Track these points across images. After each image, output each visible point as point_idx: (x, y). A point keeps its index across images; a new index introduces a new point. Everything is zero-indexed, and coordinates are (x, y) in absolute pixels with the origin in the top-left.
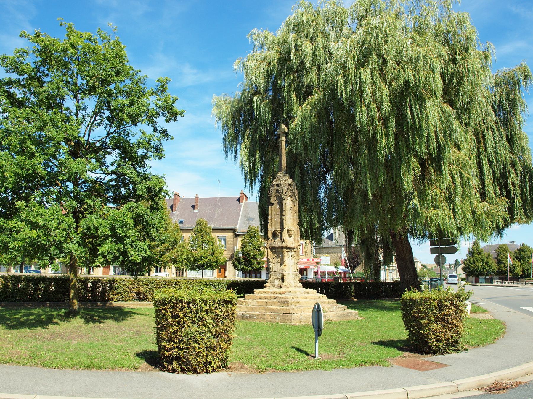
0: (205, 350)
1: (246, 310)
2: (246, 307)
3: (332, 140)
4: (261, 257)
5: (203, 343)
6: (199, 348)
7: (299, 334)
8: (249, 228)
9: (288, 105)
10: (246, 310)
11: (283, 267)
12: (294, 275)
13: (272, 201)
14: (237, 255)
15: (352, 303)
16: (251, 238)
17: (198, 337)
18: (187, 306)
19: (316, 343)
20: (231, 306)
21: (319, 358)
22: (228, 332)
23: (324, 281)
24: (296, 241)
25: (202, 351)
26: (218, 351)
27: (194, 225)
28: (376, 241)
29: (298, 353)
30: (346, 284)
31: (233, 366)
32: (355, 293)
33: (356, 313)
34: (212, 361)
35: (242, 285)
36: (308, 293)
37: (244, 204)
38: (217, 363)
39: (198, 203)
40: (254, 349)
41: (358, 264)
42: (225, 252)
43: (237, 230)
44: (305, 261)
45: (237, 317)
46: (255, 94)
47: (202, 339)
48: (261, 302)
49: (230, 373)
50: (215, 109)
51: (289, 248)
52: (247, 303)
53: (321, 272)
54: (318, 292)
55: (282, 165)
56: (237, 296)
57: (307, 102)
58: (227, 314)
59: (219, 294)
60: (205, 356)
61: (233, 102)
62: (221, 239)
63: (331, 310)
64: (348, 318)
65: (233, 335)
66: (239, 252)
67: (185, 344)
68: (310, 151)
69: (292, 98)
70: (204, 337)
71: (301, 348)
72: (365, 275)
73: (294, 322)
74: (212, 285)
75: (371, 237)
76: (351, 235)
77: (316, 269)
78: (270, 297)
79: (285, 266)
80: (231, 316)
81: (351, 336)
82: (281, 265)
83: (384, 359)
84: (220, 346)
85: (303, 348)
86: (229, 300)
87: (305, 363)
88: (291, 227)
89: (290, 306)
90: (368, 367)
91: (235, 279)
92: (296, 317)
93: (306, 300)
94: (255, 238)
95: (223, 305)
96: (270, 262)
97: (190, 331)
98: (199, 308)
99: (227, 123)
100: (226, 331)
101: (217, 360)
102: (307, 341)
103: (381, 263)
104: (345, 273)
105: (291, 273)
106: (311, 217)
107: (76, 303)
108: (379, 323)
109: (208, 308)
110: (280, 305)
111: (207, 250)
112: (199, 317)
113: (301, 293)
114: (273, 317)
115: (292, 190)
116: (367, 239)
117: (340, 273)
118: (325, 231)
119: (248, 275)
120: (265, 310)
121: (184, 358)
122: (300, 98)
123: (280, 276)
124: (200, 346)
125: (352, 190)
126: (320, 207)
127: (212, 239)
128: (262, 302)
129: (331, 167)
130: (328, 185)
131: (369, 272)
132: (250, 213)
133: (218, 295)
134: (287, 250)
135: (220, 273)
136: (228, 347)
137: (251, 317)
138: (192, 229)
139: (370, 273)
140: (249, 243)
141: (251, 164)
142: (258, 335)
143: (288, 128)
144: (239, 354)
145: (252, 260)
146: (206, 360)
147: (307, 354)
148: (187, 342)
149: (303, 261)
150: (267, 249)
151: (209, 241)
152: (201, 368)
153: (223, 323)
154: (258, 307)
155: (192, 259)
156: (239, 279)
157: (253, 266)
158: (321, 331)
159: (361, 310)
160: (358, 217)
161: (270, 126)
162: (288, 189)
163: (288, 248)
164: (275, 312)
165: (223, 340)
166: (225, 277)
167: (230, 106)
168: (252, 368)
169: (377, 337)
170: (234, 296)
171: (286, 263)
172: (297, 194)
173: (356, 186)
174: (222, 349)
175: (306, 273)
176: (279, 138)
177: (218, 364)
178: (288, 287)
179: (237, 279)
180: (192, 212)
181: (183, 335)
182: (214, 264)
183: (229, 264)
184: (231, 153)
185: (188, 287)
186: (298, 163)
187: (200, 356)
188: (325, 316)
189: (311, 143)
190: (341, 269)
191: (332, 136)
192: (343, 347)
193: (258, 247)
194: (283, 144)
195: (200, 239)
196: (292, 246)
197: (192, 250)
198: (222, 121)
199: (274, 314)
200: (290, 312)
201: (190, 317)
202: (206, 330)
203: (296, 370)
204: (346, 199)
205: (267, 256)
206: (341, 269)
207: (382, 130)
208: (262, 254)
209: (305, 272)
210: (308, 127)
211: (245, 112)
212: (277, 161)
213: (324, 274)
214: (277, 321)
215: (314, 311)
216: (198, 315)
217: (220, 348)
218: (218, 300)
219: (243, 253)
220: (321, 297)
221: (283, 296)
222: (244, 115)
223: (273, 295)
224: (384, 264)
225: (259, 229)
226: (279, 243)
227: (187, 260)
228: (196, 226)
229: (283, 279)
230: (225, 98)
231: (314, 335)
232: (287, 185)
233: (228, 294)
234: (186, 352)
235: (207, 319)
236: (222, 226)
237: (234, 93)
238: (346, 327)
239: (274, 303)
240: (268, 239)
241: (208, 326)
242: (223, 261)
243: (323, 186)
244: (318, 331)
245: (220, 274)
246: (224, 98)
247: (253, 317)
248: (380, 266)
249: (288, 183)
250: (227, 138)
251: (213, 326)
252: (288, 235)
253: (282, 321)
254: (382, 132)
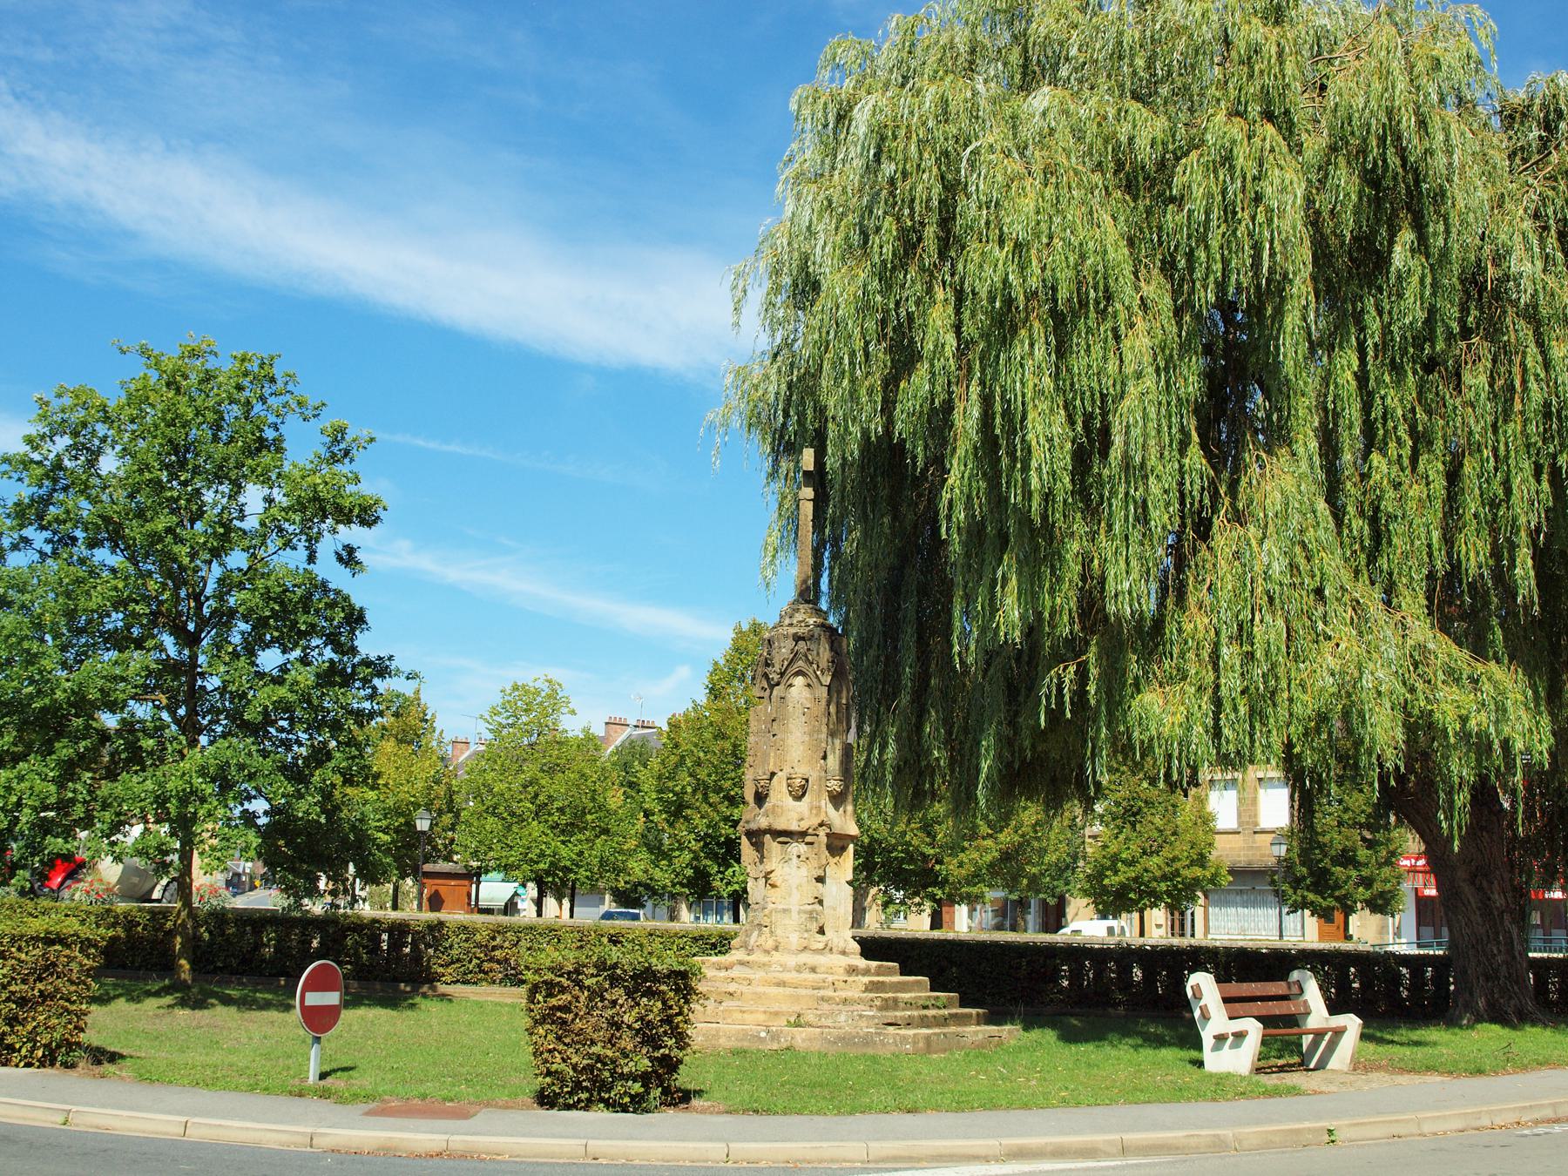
12: (805, 916)
105: (795, 909)
107: (187, 967)
166: (1348, 938)
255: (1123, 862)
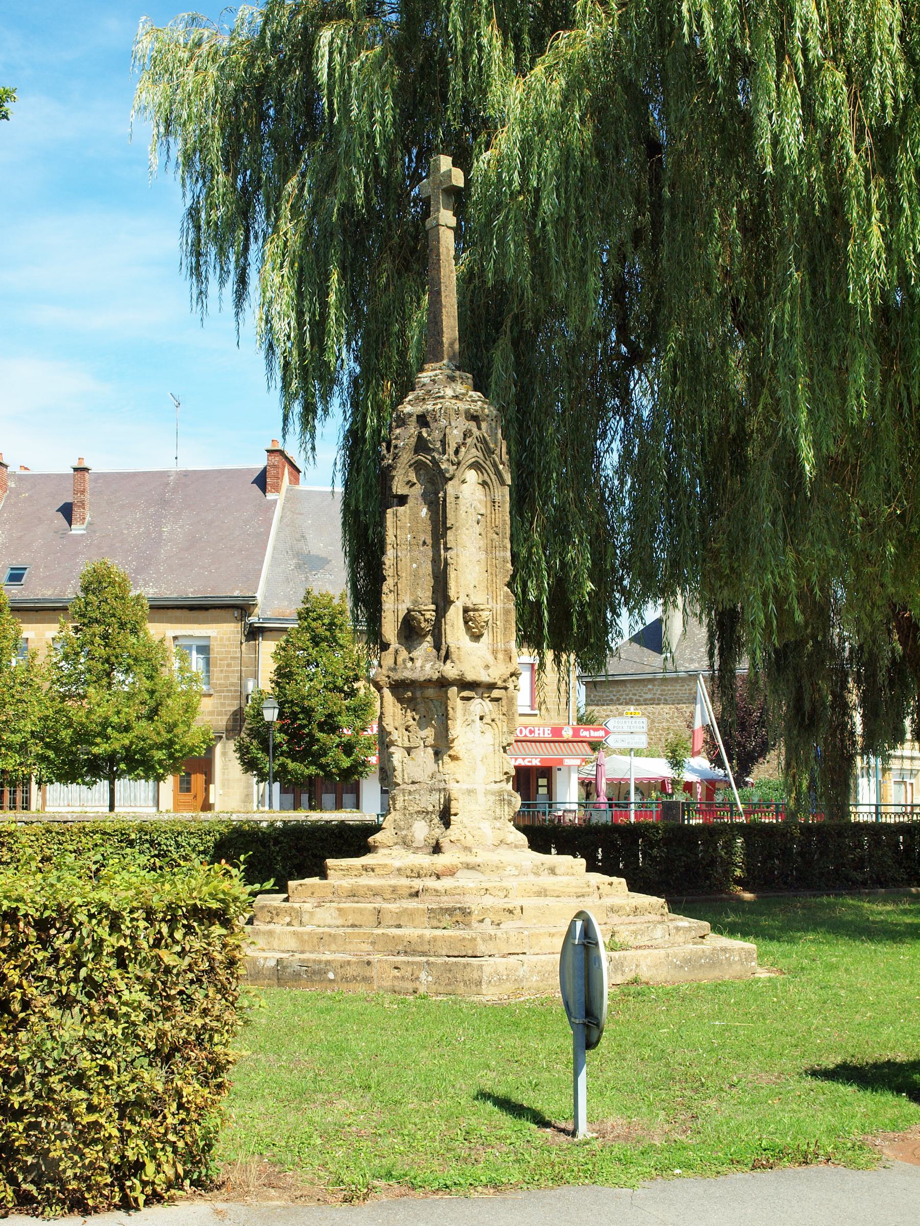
0: (116, 1116)
1: (292, 944)
2: (294, 933)
3: (656, 224)
4: (359, 723)
5: (107, 1087)
6: (91, 1109)
7: (511, 1042)
8: (306, 600)
9: (465, 67)
10: (292, 944)
11: (448, 765)
12: (492, 798)
13: (398, 488)
14: (259, 714)
15: (735, 911)
16: (316, 641)
17: (86, 1061)
18: (39, 938)
19: (576, 1075)
20: (224, 931)
21: (590, 1135)
22: (211, 1038)
23: (621, 820)
24: (500, 656)
25: (102, 1121)
26: (170, 1120)
27: (71, 591)
28: (834, 653)
29: (506, 1120)
30: (710, 832)
31: (235, 1176)
32: (748, 868)
33: (749, 953)
34: (147, 1160)
35: (277, 842)
36: (552, 871)
37: (287, 500)
38: (166, 1167)
39: (87, 497)
40: (323, 1104)
41: (764, 749)
42: (206, 705)
43: (257, 611)
44: (542, 737)
45: (256, 975)
46: (322, 18)
47: (105, 1070)
48: (354, 911)
49: (220, 1206)
50: (149, 84)
51: (473, 686)
52: (298, 916)
53: (611, 783)
54: (591, 868)
55: (440, 333)
56: (249, 888)
57: (548, 58)
58: (205, 966)
59: (173, 884)
60: (115, 1141)
61: (229, 52)
62: (189, 647)
63: (643, 941)
64: (716, 973)
65: (232, 1053)
66: (265, 704)
67: (29, 1095)
68: (558, 272)
69: (485, 41)
70: (112, 1064)
71: (518, 1097)
72: (790, 792)
73: (493, 990)
74: (152, 842)
75: (814, 637)
76: (733, 630)
77: (589, 770)
78: (394, 890)
79: (454, 758)
80: (223, 974)
81: (723, 1046)
82: (438, 754)
83: (857, 1136)
84: (181, 1097)
85: (525, 1098)
86: (215, 905)
87: (532, 1157)
88: (478, 598)
89: (475, 924)
90: (790, 1170)
91: (250, 816)
92: (501, 969)
93: (541, 901)
94: (333, 642)
95: (189, 930)
96: (392, 743)
97: (53, 1038)
98: (88, 941)
99: (202, 148)
100: (201, 1037)
101: (166, 1156)
102: (541, 1070)
103: (854, 743)
104: (711, 785)
105: (481, 788)
106: (563, 554)
108: (842, 993)
109: (126, 943)
110: (435, 923)
111: (130, 696)
112: (89, 979)
113: (521, 872)
114: (406, 972)
115: (483, 441)
116: (800, 644)
117: (689, 787)
118: (624, 611)
119: (305, 798)
120: (373, 943)
121: (29, 1150)
122: (517, 38)
123: (433, 801)
124: (95, 1101)
125: (742, 438)
126: (602, 511)
127: (150, 648)
128: (361, 911)
129: (649, 342)
130: (639, 418)
131: (805, 784)
132: (310, 536)
133: (167, 887)
134: (465, 694)
135: (188, 790)
136: (214, 1102)
137: (314, 973)
138: (65, 609)
139: (809, 788)
140: (308, 663)
141: (307, 327)
142: (340, 1050)
143: (467, 172)
144: (262, 1125)
145: (320, 735)
146: (123, 1157)
147: (542, 1122)
148: (38, 1087)
149: (536, 736)
150: (379, 688)
151: (136, 659)
152: (99, 1190)
153: (189, 1001)
154: (341, 931)
155: (66, 734)
156: (266, 816)
157: (323, 760)
158: (598, 1025)
159: (772, 938)
160: (763, 554)
161: (391, 162)
162: (467, 434)
163: (465, 685)
164: (414, 953)
165: (191, 1071)
166: (207, 806)
167: (213, 71)
168: (312, 1183)
169: (831, 1049)
170: (236, 891)
171: (458, 748)
172: (505, 457)
173: (753, 424)
174: (188, 1110)
175: (549, 786)
176: (426, 214)
177: (171, 1173)
178: (467, 849)
179: (257, 817)
180: (64, 535)
181: (24, 1055)
182: (159, 755)
183: (224, 754)
184: (222, 282)
185: (48, 853)
186: (508, 322)
187: (95, 1141)
188: (618, 967)
189: (562, 239)
190: (694, 771)
191: (657, 207)
192: (688, 1093)
193: (347, 680)
194: (447, 240)
195: (101, 652)
196: (484, 677)
197: (63, 698)
198: (180, 141)
199: (410, 959)
200: (474, 950)
201: (49, 979)
202: (118, 1032)
203: (495, 1187)
204: (712, 477)
205: (381, 718)
206: (694, 771)
207: (867, 182)
208: (360, 710)
209: (543, 781)
210: (550, 168)
211: (280, 98)
212: (420, 316)
213: (623, 792)
214: (422, 990)
215: (570, 947)
216: (83, 973)
217: (180, 1106)
218: (169, 907)
219: (281, 705)
220: (605, 889)
221: (446, 883)
222: (278, 112)
223: (404, 882)
224: (870, 747)
225: (349, 605)
226: (428, 666)
227: (42, 739)
228: (81, 594)
229: (446, 816)
230: (194, 36)
231: (568, 1043)
232: (462, 419)
233: (207, 884)
234: (35, 1126)
235: (121, 985)
236: (192, 591)
237: (232, 11)
238: (706, 1008)
239: (411, 914)
240: (385, 647)
241: (126, 1014)
242: (196, 742)
243: (617, 424)
244: (587, 1026)
245: (187, 797)
246: (188, 33)
247: (322, 973)
248: (850, 759)
249: (467, 412)
250: (203, 215)
251: (150, 1018)
252: (468, 629)
253: (441, 990)
254: (868, 191)
255: (113, 727)
